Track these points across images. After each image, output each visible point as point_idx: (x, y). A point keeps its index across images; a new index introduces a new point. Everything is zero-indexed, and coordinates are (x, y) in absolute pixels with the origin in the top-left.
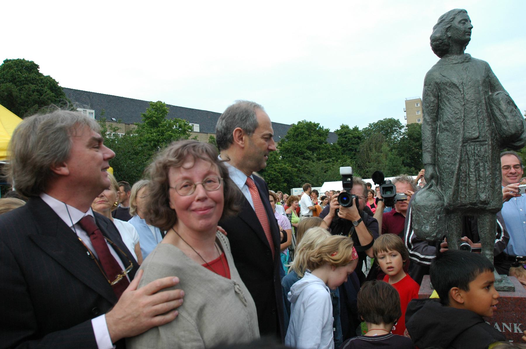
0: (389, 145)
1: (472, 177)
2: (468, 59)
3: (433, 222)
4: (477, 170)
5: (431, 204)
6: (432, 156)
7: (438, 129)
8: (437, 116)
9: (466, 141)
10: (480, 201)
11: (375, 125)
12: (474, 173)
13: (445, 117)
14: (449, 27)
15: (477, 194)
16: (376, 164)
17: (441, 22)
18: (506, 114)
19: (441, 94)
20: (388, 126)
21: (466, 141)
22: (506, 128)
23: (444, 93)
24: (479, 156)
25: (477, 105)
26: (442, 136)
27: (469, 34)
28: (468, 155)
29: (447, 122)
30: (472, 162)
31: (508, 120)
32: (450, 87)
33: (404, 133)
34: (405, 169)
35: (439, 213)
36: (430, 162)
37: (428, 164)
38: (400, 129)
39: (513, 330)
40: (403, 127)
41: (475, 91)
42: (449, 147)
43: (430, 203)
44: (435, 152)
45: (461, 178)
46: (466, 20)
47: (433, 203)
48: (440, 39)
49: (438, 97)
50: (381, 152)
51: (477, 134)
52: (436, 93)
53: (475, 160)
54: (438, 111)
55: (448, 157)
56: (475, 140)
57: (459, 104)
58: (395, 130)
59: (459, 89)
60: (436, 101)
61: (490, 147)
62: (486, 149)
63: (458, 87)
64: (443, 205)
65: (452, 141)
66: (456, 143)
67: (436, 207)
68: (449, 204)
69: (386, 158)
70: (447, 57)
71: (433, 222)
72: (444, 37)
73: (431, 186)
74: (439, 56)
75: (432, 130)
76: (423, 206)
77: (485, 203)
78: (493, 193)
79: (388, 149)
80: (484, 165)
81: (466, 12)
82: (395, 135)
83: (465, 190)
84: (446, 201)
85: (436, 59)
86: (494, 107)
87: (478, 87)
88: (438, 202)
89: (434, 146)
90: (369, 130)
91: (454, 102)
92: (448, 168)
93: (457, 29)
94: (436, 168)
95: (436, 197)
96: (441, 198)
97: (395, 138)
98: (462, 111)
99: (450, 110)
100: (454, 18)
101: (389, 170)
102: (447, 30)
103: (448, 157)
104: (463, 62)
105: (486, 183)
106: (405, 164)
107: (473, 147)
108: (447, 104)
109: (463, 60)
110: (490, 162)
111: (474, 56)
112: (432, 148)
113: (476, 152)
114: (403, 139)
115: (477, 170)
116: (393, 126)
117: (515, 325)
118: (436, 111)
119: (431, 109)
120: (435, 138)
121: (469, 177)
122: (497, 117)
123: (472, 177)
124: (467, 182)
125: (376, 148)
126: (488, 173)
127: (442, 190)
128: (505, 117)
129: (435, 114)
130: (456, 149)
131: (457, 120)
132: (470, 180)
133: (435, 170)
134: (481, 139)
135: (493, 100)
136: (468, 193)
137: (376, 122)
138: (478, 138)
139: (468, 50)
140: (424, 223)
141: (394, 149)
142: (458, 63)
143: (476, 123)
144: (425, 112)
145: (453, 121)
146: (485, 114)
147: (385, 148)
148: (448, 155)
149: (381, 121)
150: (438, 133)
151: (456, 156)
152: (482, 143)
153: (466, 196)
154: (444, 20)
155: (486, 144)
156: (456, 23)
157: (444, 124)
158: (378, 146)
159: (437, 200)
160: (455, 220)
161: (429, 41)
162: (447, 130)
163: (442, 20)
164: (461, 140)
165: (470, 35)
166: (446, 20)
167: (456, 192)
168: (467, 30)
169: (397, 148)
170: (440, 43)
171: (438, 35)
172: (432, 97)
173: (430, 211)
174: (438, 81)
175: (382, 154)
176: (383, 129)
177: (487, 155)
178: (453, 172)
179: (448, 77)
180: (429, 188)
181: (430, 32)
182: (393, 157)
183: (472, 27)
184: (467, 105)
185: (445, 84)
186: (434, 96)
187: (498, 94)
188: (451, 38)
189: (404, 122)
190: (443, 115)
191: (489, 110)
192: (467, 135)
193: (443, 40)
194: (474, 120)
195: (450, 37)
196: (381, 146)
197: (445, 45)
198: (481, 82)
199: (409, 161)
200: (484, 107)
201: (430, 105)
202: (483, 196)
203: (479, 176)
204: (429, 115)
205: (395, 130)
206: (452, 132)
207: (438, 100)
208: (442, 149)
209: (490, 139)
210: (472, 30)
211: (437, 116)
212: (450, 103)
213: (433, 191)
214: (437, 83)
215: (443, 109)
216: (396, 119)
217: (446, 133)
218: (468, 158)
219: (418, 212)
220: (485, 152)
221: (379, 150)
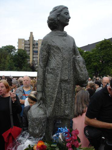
0: (10, 57)
1: (63, 102)
2: (65, 35)
3: (41, 128)
4: (65, 97)
5: (40, 117)
6: (42, 87)
7: (47, 71)
8: (47, 64)
9: (62, 81)
10: (65, 115)
11: (5, 47)
12: (63, 99)
13: (51, 65)
14: (59, 14)
15: (64, 111)
16: (3, 65)
17: (55, 10)
18: (82, 69)
19: (50, 51)
20: (10, 48)
21: (62, 81)
22: (81, 77)
23: (52, 51)
24: (67, 90)
25: (69, 62)
26: (49, 76)
27: (68, 21)
28: (61, 88)
29: (52, 69)
30: (63, 93)
31: (83, 73)
32: (56, 49)
33: (16, 53)
34: (15, 68)
35: (44, 122)
36: (41, 91)
37: (40, 91)
38: (15, 50)
40: (16, 50)
41: (68, 54)
42: (52, 84)
43: (40, 116)
44: (44, 84)
45: (58, 102)
46: (67, 13)
47: (41, 116)
48: (54, 20)
49: (49, 53)
50: (6, 60)
51: (67, 78)
52: (48, 51)
53: (65, 92)
54: (47, 61)
55: (51, 89)
56: (66, 81)
57: (60, 59)
58: (13, 51)
59: (61, 51)
60: (47, 55)
61: (73, 86)
62: (69, 86)
63: (60, 50)
64: (46, 117)
65: (54, 80)
66: (56, 81)
67: (43, 119)
68: (50, 117)
69: (8, 62)
70: (55, 31)
71: (41, 128)
72: (56, 20)
73: (40, 104)
74: (51, 29)
75: (43, 72)
76: (36, 118)
77: (68, 116)
78: (71, 110)
79: (9, 58)
80: (69, 95)
81: (67, 8)
82: (13, 53)
83: (58, 108)
84: (48, 114)
85: (49, 31)
86: (77, 64)
87: (70, 52)
88: (44, 116)
89: (44, 81)
90: (2, 49)
91: (57, 58)
92: (50, 95)
93: (63, 16)
94: (43, 94)
95: (43, 113)
96: (46, 113)
97: (13, 54)
98: (61, 64)
99: (54, 62)
100: (62, 10)
101: (9, 68)
102: (58, 15)
103: (51, 89)
104: (64, 36)
105: (69, 105)
106: (15, 66)
107: (64, 85)
108: (53, 58)
109: (64, 35)
110: (72, 94)
111: (69, 33)
112: (42, 82)
113: (66, 88)
114: (16, 55)
116: (12, 49)
118: (46, 61)
119: (44, 59)
120: (45, 76)
121: (61, 101)
122: (77, 70)
123: (63, 102)
124: (60, 104)
125: (4, 57)
126: (70, 100)
127: (45, 106)
128: (82, 71)
129: (46, 63)
130: (56, 85)
131: (58, 69)
132: (61, 103)
133: (43, 95)
134: (69, 81)
135: (76, 60)
136: (59, 110)
137: (5, 46)
138: (67, 80)
139: (66, 29)
140: (36, 129)
141: (12, 59)
142: (61, 36)
143: (67, 72)
144: (40, 60)
145: (56, 68)
146: (72, 67)
147: (8, 58)
148: (51, 88)
149: (7, 46)
150: (46, 74)
151: (56, 89)
152: (69, 83)
153: (58, 112)
154: (56, 10)
155: (70, 84)
156: (62, 13)
157: (51, 69)
158: (5, 56)
159: (44, 115)
160: (51, 124)
161: (47, 19)
162: (52, 74)
163: (55, 9)
164: (59, 80)
165: (68, 22)
166: (58, 10)
167: (54, 110)
168: (68, 19)
169: (13, 59)
170: (54, 22)
171: (53, 17)
172: (45, 53)
173: (40, 121)
174: (50, 44)
175: (6, 60)
176: (8, 49)
177: (71, 89)
178: (53, 98)
179: (56, 43)
180: (39, 106)
181: (48, 15)
182: (11, 62)
183: (70, 18)
184: (64, 61)
185: (54, 46)
186: (47, 52)
187: (79, 57)
188: (31, 33)
189: (17, 48)
190: (50, 64)
191: (74, 65)
192: (63, 78)
193: (55, 21)
194: (66, 70)
195: (59, 20)
196: (6, 57)
197: (56, 24)
198: (71, 49)
199: (17, 65)
200: (72, 63)
201: (44, 57)
202: (67, 112)
203: (66, 101)
204: (42, 63)
205: (13, 51)
206: (55, 75)
207: (48, 54)
208: (48, 84)
209: (73, 81)
210: (70, 19)
211: (47, 64)
212: (55, 58)
213: (41, 108)
214: (48, 45)
215: (50, 60)
216: (14, 46)
217: (51, 75)
218: (62, 91)
219: (33, 122)
220: (70, 88)
221: (5, 58)
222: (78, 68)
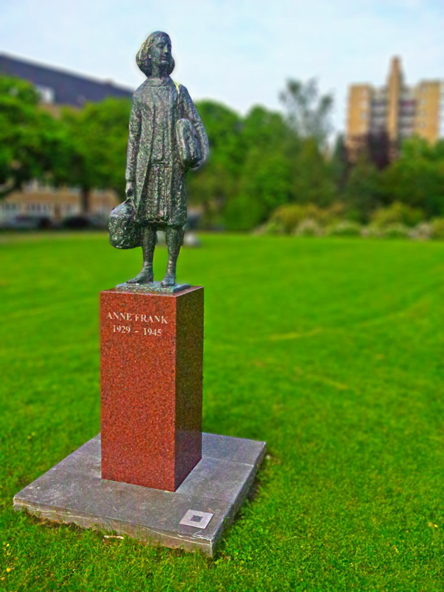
4: (159, 190)
39: (161, 321)
117: (162, 317)
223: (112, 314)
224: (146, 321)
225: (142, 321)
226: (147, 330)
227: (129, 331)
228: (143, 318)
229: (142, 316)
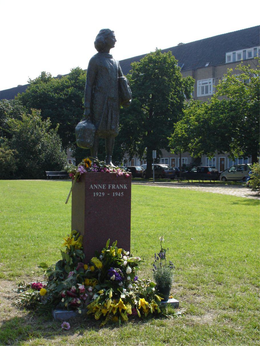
4: (112, 114)
39: (124, 188)
115: (112, 114)
117: (125, 185)
183: (116, 41)
222: (123, 88)
223: (119, 186)
224: (115, 188)
225: (113, 188)
226: (95, 194)
227: (104, 195)
228: (113, 187)
229: (113, 185)
